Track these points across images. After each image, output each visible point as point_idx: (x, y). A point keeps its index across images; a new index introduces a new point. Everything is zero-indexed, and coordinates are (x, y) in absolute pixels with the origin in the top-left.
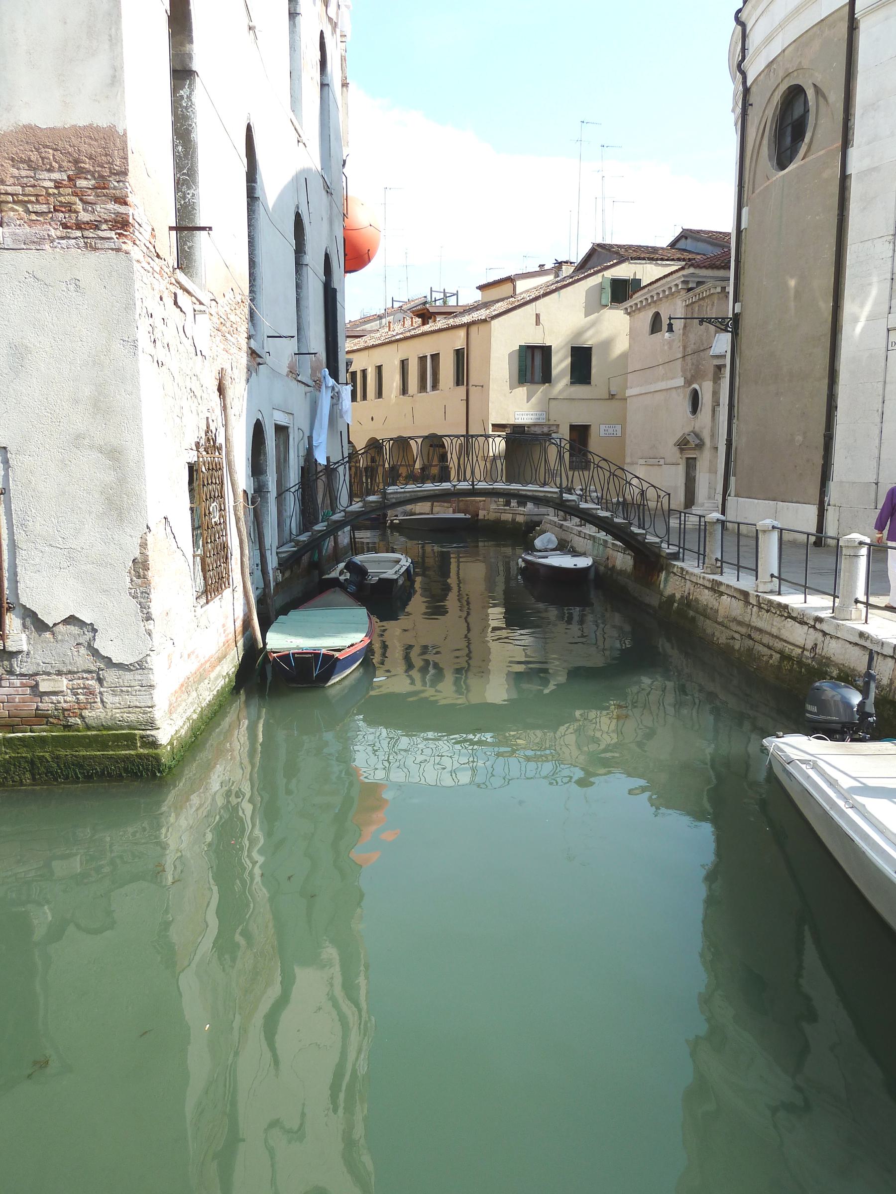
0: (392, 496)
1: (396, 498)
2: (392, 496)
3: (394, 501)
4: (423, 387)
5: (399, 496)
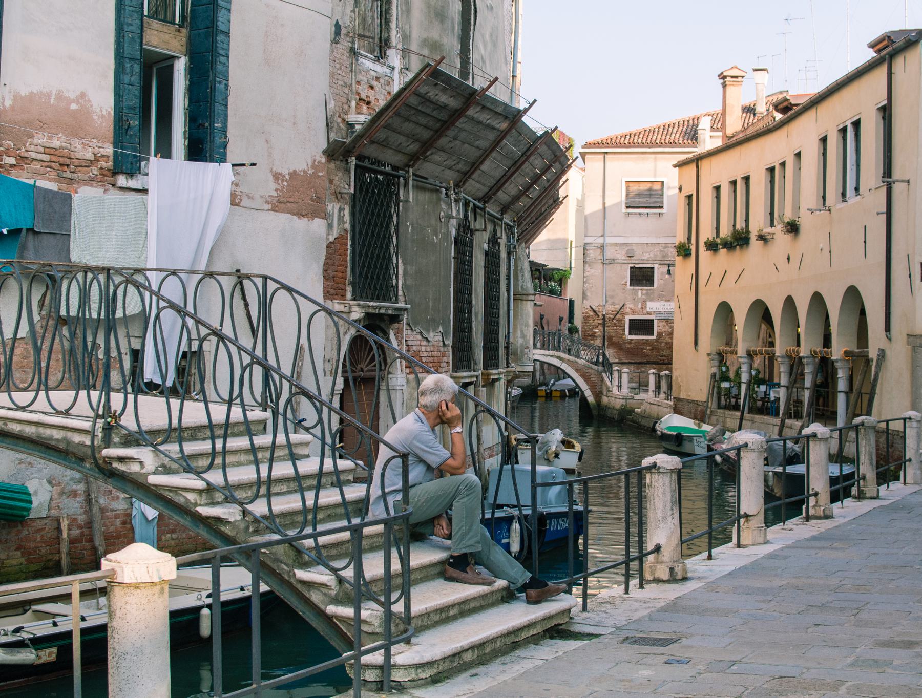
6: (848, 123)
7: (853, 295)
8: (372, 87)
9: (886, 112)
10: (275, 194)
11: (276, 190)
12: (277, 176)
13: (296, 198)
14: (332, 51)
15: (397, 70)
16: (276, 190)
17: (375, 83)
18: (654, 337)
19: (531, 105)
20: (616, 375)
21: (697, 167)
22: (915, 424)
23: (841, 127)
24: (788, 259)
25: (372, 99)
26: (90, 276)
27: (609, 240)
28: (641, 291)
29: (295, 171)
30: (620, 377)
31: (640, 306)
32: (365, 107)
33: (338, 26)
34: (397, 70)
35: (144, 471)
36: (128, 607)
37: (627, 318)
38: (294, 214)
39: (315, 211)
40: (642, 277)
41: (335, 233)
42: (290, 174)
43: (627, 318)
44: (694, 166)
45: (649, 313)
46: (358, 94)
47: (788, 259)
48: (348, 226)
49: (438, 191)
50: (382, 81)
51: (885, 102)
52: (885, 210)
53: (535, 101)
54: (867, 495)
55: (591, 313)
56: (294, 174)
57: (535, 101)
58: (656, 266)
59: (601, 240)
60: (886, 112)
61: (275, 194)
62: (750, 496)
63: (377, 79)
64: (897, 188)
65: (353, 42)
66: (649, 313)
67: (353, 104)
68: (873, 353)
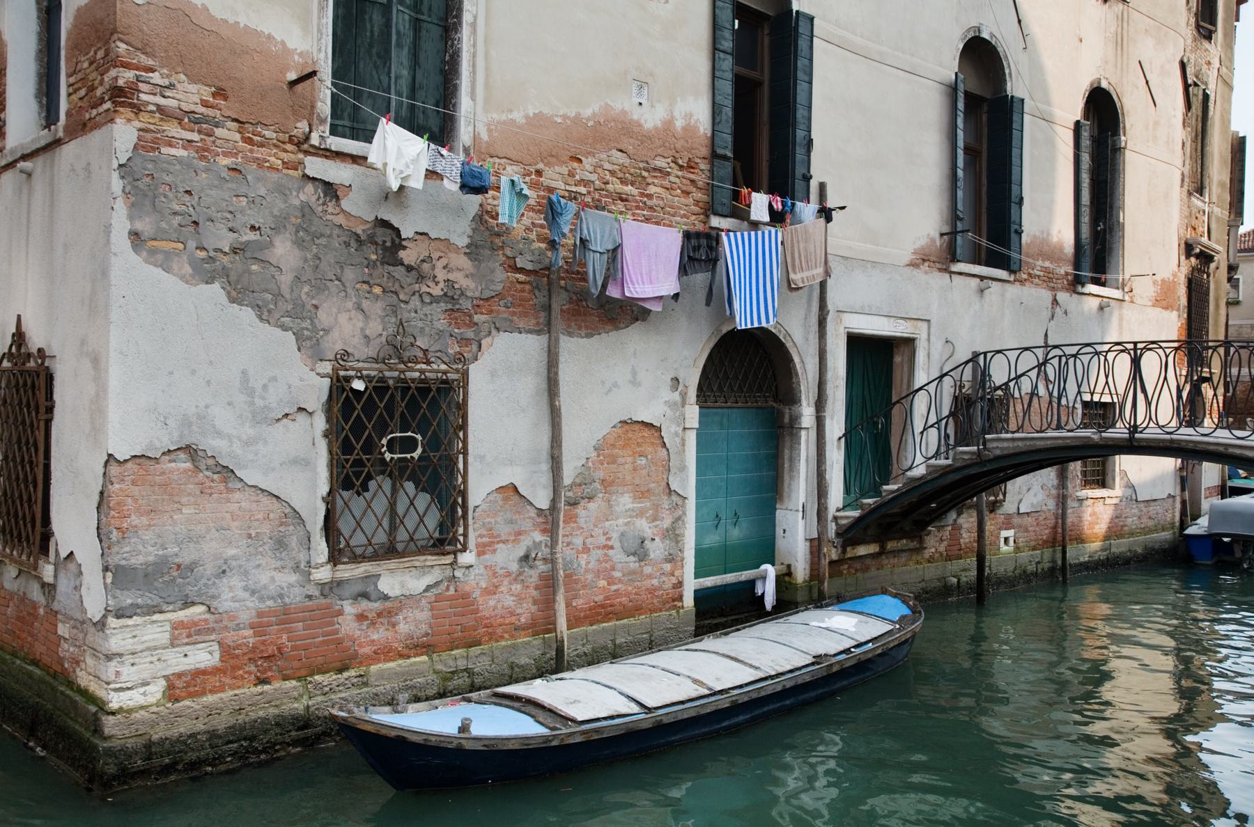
0: (995, 444)
1: (1002, 449)
2: (995, 444)
3: (998, 452)
5: (1005, 444)
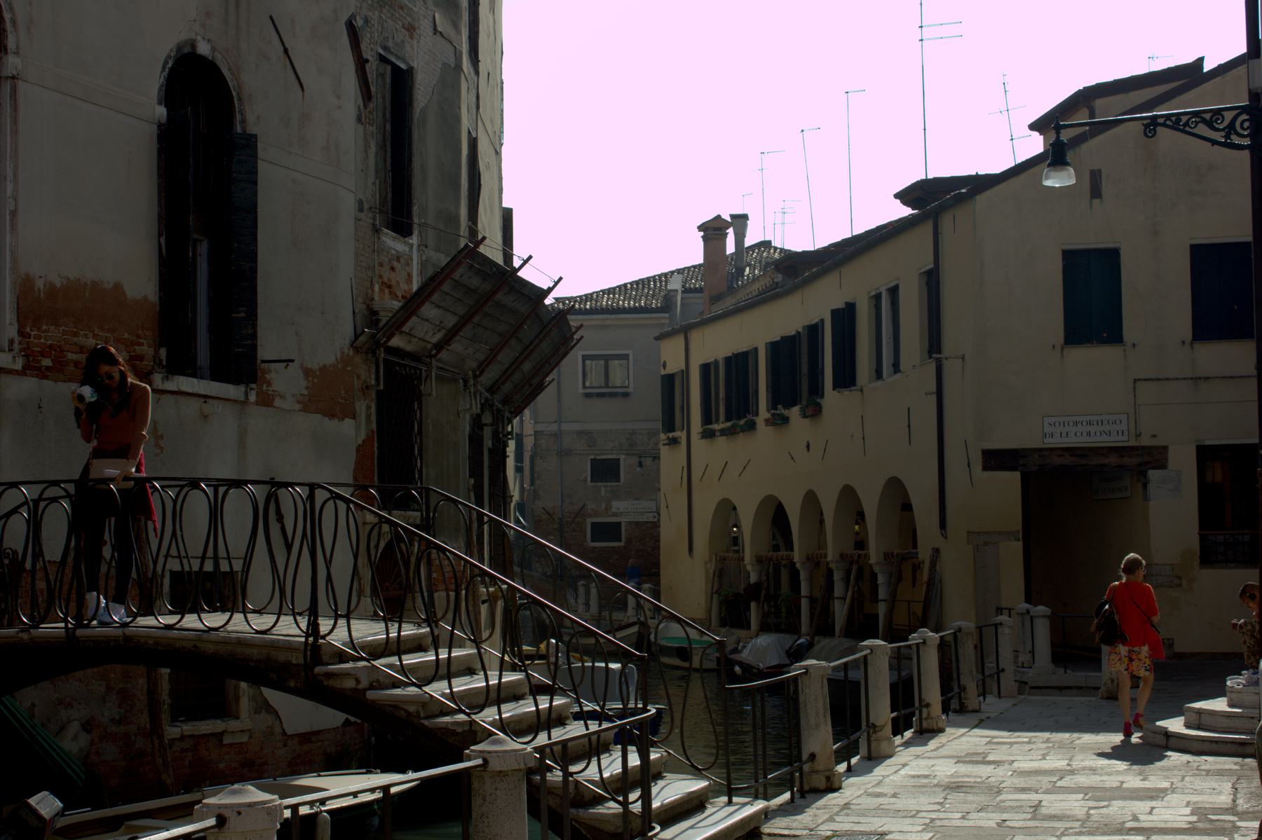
4: (894, 291)
6: (883, 290)
7: (895, 487)
8: (393, 269)
9: (932, 280)
10: (306, 392)
11: (307, 388)
12: (307, 372)
13: (325, 397)
14: (356, 229)
15: (415, 248)
16: (307, 388)
17: (395, 264)
18: (622, 544)
19: (556, 283)
20: (581, 590)
21: (686, 339)
22: (1007, 631)
23: (873, 293)
24: (808, 447)
25: (393, 283)
26: (222, 490)
27: (565, 427)
28: (604, 488)
29: (324, 366)
30: (588, 593)
31: (603, 506)
32: (387, 291)
33: (361, 202)
34: (415, 248)
35: (360, 687)
36: (498, 792)
37: (589, 521)
38: (325, 415)
39: (339, 411)
40: (605, 470)
41: (363, 436)
42: (320, 369)
43: (589, 521)
44: (680, 340)
45: (615, 515)
46: (381, 277)
47: (808, 447)
48: (374, 426)
49: (456, 380)
50: (402, 260)
51: (931, 266)
52: (934, 390)
53: (561, 279)
54: (970, 708)
55: (545, 517)
56: (323, 368)
57: (561, 279)
58: (622, 457)
59: (554, 427)
60: (932, 280)
61: (306, 392)
62: (881, 710)
63: (398, 259)
64: (950, 368)
65: (374, 219)
66: (615, 515)
67: (377, 288)
68: (924, 554)
